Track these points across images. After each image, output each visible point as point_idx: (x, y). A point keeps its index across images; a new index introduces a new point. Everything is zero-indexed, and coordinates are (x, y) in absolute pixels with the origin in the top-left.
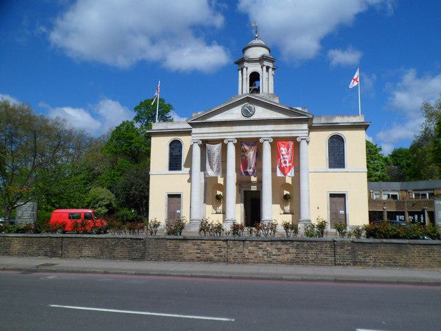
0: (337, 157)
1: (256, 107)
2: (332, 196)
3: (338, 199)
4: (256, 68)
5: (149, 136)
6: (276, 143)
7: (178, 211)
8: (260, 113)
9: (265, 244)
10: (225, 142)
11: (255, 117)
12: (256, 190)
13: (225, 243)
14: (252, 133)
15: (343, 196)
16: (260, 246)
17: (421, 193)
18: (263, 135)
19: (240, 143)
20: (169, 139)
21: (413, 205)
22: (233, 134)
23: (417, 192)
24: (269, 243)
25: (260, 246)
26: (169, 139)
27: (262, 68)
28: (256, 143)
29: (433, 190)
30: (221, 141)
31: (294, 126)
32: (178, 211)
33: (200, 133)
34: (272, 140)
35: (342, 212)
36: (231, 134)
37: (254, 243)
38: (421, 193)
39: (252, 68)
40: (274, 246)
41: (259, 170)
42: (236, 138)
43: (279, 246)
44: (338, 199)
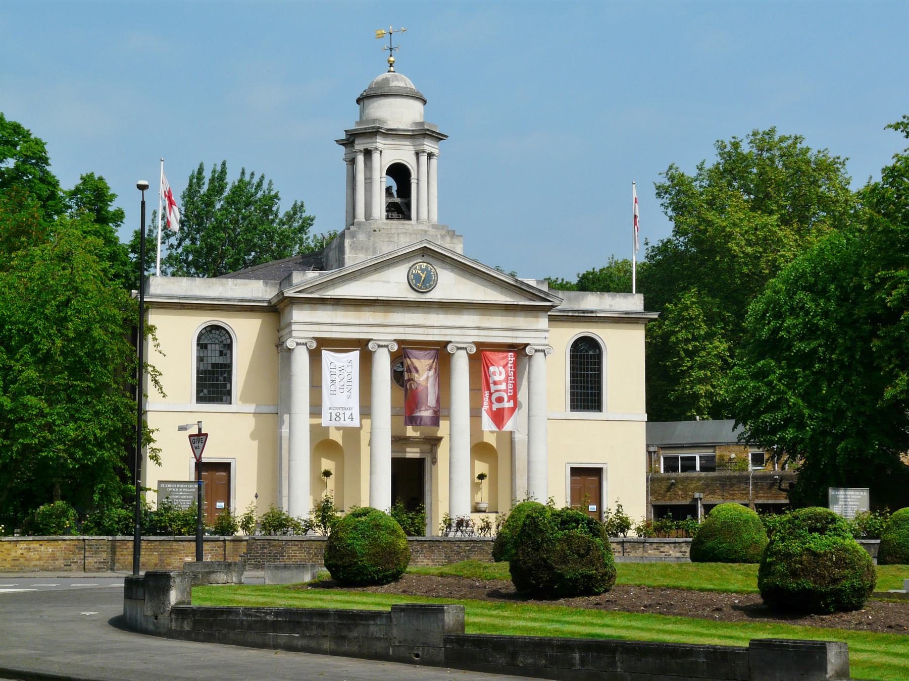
0: (586, 391)
1: (439, 270)
2: (575, 471)
3: (588, 478)
4: (403, 154)
5: (143, 309)
6: (481, 356)
7: (220, 505)
8: (450, 286)
9: (667, 546)
10: (371, 346)
11: (435, 295)
12: (417, 456)
13: (619, 546)
14: (430, 331)
15: (597, 472)
16: (662, 549)
17: (682, 454)
18: (454, 337)
19: (402, 355)
20: (197, 322)
21: (669, 489)
22: (389, 330)
23: (671, 453)
24: (672, 545)
25: (662, 549)
26: (197, 322)
27: (417, 154)
28: (441, 353)
29: (713, 446)
30: (362, 345)
31: (521, 321)
32: (220, 505)
33: (332, 324)
34: (474, 350)
35: (593, 508)
36: (386, 330)
37: (655, 546)
38: (682, 454)
39: (390, 153)
40: (677, 549)
41: (442, 411)
42: (395, 340)
43: (683, 549)
44: (588, 478)
